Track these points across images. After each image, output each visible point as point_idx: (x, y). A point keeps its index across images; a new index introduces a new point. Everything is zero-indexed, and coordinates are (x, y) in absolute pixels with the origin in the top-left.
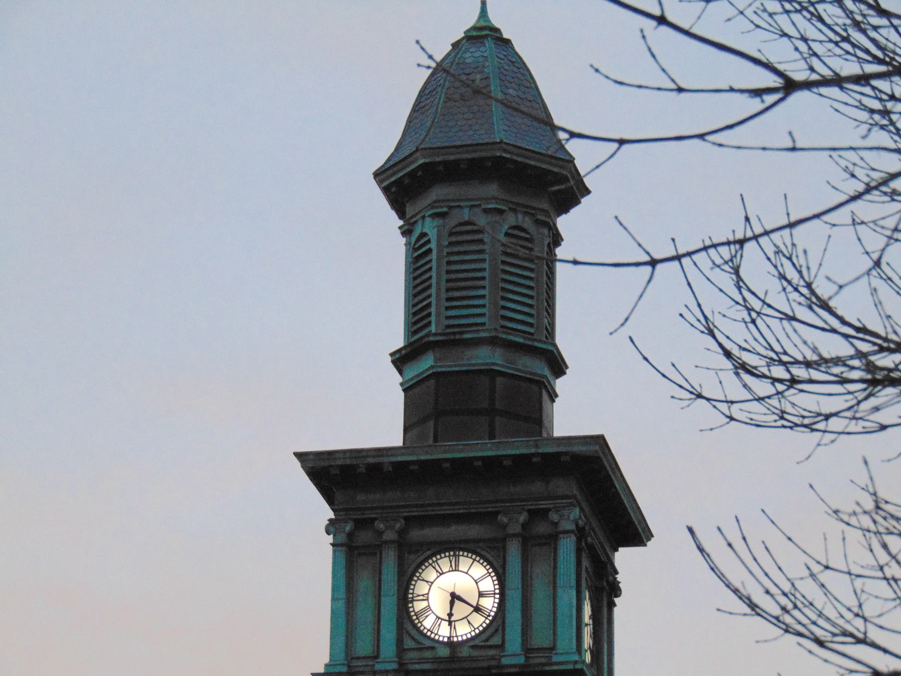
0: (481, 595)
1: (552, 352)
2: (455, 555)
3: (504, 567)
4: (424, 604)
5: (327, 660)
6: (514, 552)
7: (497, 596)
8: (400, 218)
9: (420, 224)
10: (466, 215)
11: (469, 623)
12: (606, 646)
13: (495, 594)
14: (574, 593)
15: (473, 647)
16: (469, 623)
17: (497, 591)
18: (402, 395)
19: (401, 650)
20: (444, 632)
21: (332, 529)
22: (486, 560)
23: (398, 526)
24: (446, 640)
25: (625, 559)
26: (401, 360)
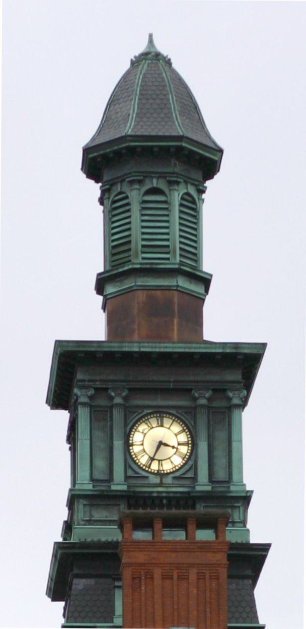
2: (160, 416)
3: (195, 426)
6: (118, 415)
7: (190, 445)
8: (97, 182)
9: (119, 185)
10: (154, 183)
11: (172, 462)
15: (174, 478)
16: (172, 462)
17: (190, 442)
19: (127, 478)
22: (182, 420)
24: (156, 472)
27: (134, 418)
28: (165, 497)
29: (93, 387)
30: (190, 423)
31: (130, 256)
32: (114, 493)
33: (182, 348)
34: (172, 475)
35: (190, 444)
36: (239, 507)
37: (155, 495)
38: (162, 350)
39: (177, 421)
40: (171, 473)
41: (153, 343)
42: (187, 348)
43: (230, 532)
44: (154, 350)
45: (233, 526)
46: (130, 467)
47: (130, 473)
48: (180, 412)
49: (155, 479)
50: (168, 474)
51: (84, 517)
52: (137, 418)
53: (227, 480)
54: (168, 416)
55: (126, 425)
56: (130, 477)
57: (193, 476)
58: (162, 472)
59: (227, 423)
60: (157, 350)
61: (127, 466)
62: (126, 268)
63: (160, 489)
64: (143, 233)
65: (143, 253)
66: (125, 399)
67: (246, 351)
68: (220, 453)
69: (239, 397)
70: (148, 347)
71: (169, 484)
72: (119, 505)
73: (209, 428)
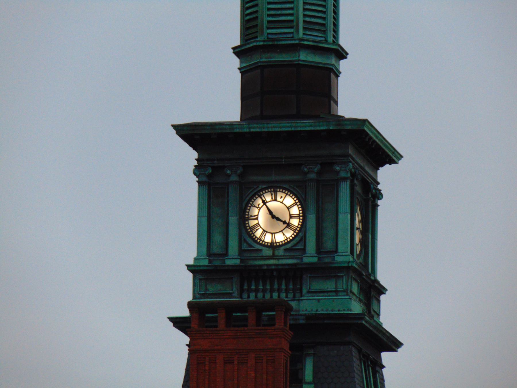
0: (291, 217)
1: (337, 50)
3: (305, 201)
4: (256, 222)
5: (195, 255)
6: (233, 194)
12: (370, 236)
13: (300, 216)
14: (349, 215)
15: (286, 250)
18: (238, 76)
19: (241, 251)
20: (268, 239)
21: (197, 173)
23: (239, 172)
25: (385, 175)
26: (238, 52)
27: (250, 193)
28: (275, 269)
29: (210, 166)
30: (302, 197)
31: (257, 32)
32: (226, 268)
33: (288, 127)
34: (283, 247)
35: (301, 216)
36: (342, 276)
37: (265, 267)
38: (270, 130)
39: (289, 195)
40: (283, 245)
41: (261, 124)
42: (293, 127)
43: (333, 301)
44: (263, 130)
45: (337, 295)
46: (245, 241)
47: (245, 246)
48: (292, 186)
49: (268, 252)
50: (280, 246)
51: (200, 291)
52: (253, 193)
53: (334, 250)
54: (281, 190)
55: (241, 199)
56: (245, 251)
57: (303, 247)
58: (275, 244)
59: (335, 196)
60: (266, 130)
61: (241, 240)
62: (251, 45)
63: (271, 262)
64: (269, 9)
65: (268, 28)
66: (241, 176)
67: (349, 127)
68: (328, 225)
69: (346, 170)
70: (257, 127)
71: (281, 256)
72: (232, 278)
73: (318, 201)
